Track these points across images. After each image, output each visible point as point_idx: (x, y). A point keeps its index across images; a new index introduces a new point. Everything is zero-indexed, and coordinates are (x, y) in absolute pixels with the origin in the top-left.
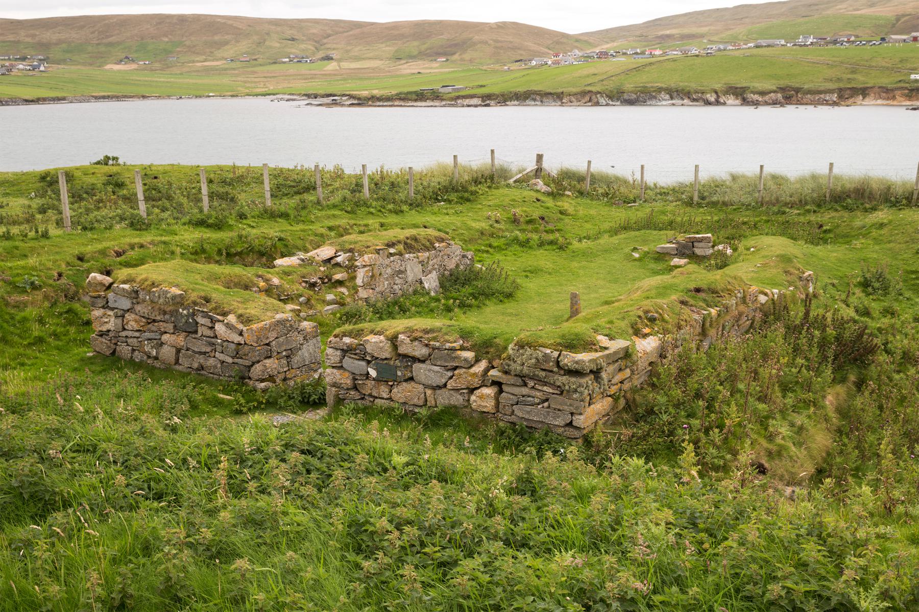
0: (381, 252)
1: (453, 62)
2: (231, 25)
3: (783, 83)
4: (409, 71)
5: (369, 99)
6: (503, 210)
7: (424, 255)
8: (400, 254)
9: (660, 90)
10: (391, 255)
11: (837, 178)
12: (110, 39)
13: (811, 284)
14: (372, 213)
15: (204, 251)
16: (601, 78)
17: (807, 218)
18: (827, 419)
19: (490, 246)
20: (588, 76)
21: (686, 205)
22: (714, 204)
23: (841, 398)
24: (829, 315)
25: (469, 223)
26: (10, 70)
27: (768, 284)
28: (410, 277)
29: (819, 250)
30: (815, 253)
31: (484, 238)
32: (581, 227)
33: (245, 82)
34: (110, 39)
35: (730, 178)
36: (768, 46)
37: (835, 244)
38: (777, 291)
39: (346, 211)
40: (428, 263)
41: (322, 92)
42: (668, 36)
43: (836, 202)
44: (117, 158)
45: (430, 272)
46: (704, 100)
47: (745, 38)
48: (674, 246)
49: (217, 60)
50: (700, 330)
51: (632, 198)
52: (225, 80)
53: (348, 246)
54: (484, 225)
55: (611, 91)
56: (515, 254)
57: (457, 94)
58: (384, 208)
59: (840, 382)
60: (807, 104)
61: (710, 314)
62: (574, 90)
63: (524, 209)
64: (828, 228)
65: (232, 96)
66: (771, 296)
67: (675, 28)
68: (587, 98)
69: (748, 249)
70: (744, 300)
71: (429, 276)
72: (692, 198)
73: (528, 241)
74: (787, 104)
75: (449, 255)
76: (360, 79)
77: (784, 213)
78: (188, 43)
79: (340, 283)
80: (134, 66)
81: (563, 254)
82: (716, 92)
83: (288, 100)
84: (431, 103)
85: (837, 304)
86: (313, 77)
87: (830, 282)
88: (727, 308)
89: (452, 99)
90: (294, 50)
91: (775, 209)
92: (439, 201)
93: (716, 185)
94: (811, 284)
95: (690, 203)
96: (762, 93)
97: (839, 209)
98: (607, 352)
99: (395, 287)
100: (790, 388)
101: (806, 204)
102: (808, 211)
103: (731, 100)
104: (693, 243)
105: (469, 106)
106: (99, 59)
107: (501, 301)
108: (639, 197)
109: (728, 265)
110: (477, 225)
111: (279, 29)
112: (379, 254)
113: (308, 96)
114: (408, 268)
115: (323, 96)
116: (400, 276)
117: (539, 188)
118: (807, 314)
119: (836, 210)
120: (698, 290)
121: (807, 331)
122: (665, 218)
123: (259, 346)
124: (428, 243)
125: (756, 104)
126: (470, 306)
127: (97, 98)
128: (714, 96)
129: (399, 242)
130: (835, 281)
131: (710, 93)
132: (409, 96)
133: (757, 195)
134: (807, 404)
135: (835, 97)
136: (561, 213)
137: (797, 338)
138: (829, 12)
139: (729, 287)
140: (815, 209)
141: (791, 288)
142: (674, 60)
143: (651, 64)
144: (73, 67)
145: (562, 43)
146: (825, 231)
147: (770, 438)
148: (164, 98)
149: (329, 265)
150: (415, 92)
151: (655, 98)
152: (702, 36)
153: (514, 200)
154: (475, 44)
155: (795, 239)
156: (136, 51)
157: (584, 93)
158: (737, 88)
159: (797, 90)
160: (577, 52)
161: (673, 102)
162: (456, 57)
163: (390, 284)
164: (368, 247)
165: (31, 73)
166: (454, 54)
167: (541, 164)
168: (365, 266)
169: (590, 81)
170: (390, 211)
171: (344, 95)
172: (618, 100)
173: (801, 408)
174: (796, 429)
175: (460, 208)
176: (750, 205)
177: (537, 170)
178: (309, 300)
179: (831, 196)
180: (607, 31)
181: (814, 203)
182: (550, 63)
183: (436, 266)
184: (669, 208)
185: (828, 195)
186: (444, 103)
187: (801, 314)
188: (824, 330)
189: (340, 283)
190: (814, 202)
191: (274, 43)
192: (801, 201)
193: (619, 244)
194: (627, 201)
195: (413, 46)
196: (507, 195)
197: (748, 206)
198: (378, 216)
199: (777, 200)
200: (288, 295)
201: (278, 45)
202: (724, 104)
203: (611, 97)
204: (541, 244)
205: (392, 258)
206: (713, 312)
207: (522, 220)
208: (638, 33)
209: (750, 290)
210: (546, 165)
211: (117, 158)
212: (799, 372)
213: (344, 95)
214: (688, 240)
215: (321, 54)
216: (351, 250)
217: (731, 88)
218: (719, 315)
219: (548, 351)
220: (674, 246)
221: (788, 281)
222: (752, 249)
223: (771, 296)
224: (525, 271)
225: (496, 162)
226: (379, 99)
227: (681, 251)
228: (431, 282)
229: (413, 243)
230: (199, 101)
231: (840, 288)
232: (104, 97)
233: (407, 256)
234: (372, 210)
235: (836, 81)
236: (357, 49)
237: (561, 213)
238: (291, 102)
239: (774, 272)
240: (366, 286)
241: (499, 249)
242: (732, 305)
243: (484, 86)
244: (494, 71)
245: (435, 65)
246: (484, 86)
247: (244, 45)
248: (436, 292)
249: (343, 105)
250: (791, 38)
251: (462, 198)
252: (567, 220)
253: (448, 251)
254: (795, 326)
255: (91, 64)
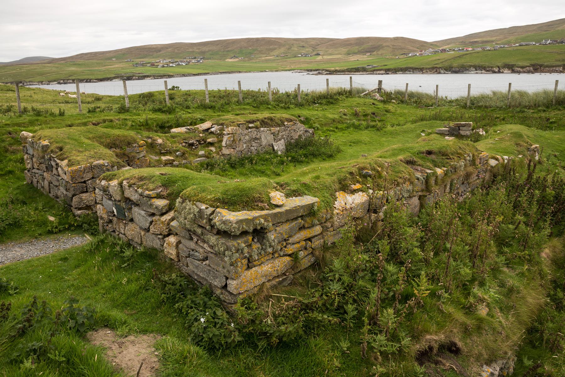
0: (241, 126)
1: (374, 55)
2: (277, 42)
3: (533, 62)
4: (353, 59)
5: (334, 71)
6: (351, 109)
7: (275, 129)
8: (257, 128)
9: (470, 66)
10: (250, 128)
11: (561, 92)
12: (229, 49)
13: (537, 154)
14: (269, 108)
15: (147, 124)
16: (441, 61)
17: (539, 115)
18: (542, 276)
19: (337, 128)
20: (435, 60)
21: (463, 108)
22: (480, 107)
23: (557, 250)
24: (550, 178)
25: (327, 115)
26: (189, 63)
27: (501, 152)
28: (264, 142)
29: (547, 134)
30: (543, 135)
31: (335, 123)
32: (397, 119)
33: (282, 65)
34: (229, 49)
35: (492, 94)
36: (526, 45)
37: (558, 130)
38: (507, 157)
39: (253, 107)
40: (278, 134)
41: (314, 69)
42: (476, 42)
43: (560, 105)
44: (179, 87)
45: (280, 140)
46: (492, 71)
47: (514, 42)
48: (447, 129)
49: (271, 56)
50: (424, 187)
51: (430, 104)
52: (274, 64)
53: (221, 122)
54: (336, 116)
55: (447, 67)
56: (349, 133)
57: (374, 69)
58: (278, 105)
59: (557, 236)
60: (546, 72)
61: (435, 174)
62: (429, 67)
63: (364, 108)
64: (553, 120)
65: (276, 71)
66: (501, 161)
67: (479, 38)
68: (435, 70)
69: (496, 132)
70: (473, 163)
71: (279, 142)
72: (466, 104)
73: (359, 125)
74: (535, 72)
75: (295, 130)
76: (332, 63)
77: (523, 112)
78: (259, 49)
79: (211, 144)
80: (237, 60)
81: (379, 133)
82: (499, 67)
83: (299, 72)
84: (362, 73)
85: (557, 169)
86: (311, 62)
87: (553, 153)
88: (455, 169)
89: (371, 71)
90: (304, 51)
91: (518, 109)
92: (316, 103)
93: (483, 97)
94: (537, 154)
95: (465, 107)
96: (522, 67)
97: (562, 109)
98: (278, 210)
99: (252, 148)
100: (507, 242)
101: (539, 106)
102: (540, 111)
103: (506, 71)
104: (459, 127)
105: (379, 74)
106: (223, 57)
107: (324, 159)
108: (435, 103)
109: (480, 141)
110: (331, 116)
111: (297, 42)
112: (239, 127)
113: (308, 70)
114: (263, 137)
115: (315, 70)
116: (256, 141)
117: (376, 98)
118: (530, 176)
119: (560, 110)
120: (429, 153)
121: (527, 191)
122: (447, 115)
123: (74, 183)
124: (280, 122)
125: (519, 72)
126: (302, 162)
127: (221, 73)
128: (498, 69)
129: (258, 120)
130: (557, 153)
131: (496, 67)
132: (352, 70)
133: (506, 102)
134: (522, 260)
135: (561, 69)
136: (386, 111)
137: (519, 196)
138: (559, 28)
139: (459, 151)
140: (545, 109)
141: (520, 156)
142: (478, 52)
143: (466, 54)
144: (213, 61)
145: (424, 46)
146: (551, 123)
147: (469, 310)
148: (248, 72)
149: (207, 133)
150: (355, 68)
151: (468, 70)
152: (493, 41)
153: (359, 104)
154: (383, 47)
155: (530, 127)
156: (238, 53)
157: (433, 68)
158: (509, 65)
159: (541, 66)
160: (431, 49)
161: (477, 72)
162: (375, 53)
163: (248, 146)
164: (234, 122)
165: (197, 64)
166: (374, 51)
167: (381, 86)
168: (229, 134)
169: (436, 62)
170: (282, 108)
171: (324, 70)
172: (450, 71)
173: (515, 263)
174: (505, 290)
175: (326, 107)
176: (502, 107)
177: (378, 89)
178: (184, 154)
179: (556, 101)
180: (446, 40)
181: (544, 106)
182: (418, 55)
183: (285, 136)
184: (452, 109)
185: (554, 101)
186: (368, 73)
187: (525, 176)
188: (544, 190)
189: (211, 144)
190: (544, 105)
191: (295, 49)
192: (535, 105)
193: (414, 128)
194: (427, 106)
195: (356, 48)
196: (356, 101)
197: (501, 108)
198: (273, 110)
199: (520, 104)
200: (167, 150)
201: (297, 49)
202: (503, 72)
203: (446, 70)
204: (367, 128)
205: (250, 130)
206: (439, 171)
207: (360, 114)
208: (461, 41)
209: (480, 155)
210: (383, 86)
211: (179, 87)
212: (516, 228)
213: (324, 70)
214: (456, 125)
215: (315, 53)
216: (222, 124)
217: (506, 65)
218: (446, 174)
219: (203, 207)
220: (447, 129)
221: (518, 151)
222: (498, 132)
223: (501, 161)
224: (351, 142)
225: (353, 86)
226: (339, 71)
227: (451, 132)
228: (279, 147)
229: (269, 122)
230: (262, 73)
231: (560, 158)
232: (224, 73)
233: (262, 129)
234: (269, 106)
235: (562, 61)
236: (330, 50)
237: (386, 111)
238: (301, 73)
239: (508, 144)
240: (227, 146)
241: (342, 129)
242: (461, 166)
243: (386, 65)
244: (392, 59)
245: (365, 56)
246: (386, 65)
247: (282, 50)
248: (282, 152)
249: (323, 74)
250: (539, 41)
251: (328, 102)
252: (388, 115)
253: (294, 127)
254: (518, 186)
255: (220, 59)
